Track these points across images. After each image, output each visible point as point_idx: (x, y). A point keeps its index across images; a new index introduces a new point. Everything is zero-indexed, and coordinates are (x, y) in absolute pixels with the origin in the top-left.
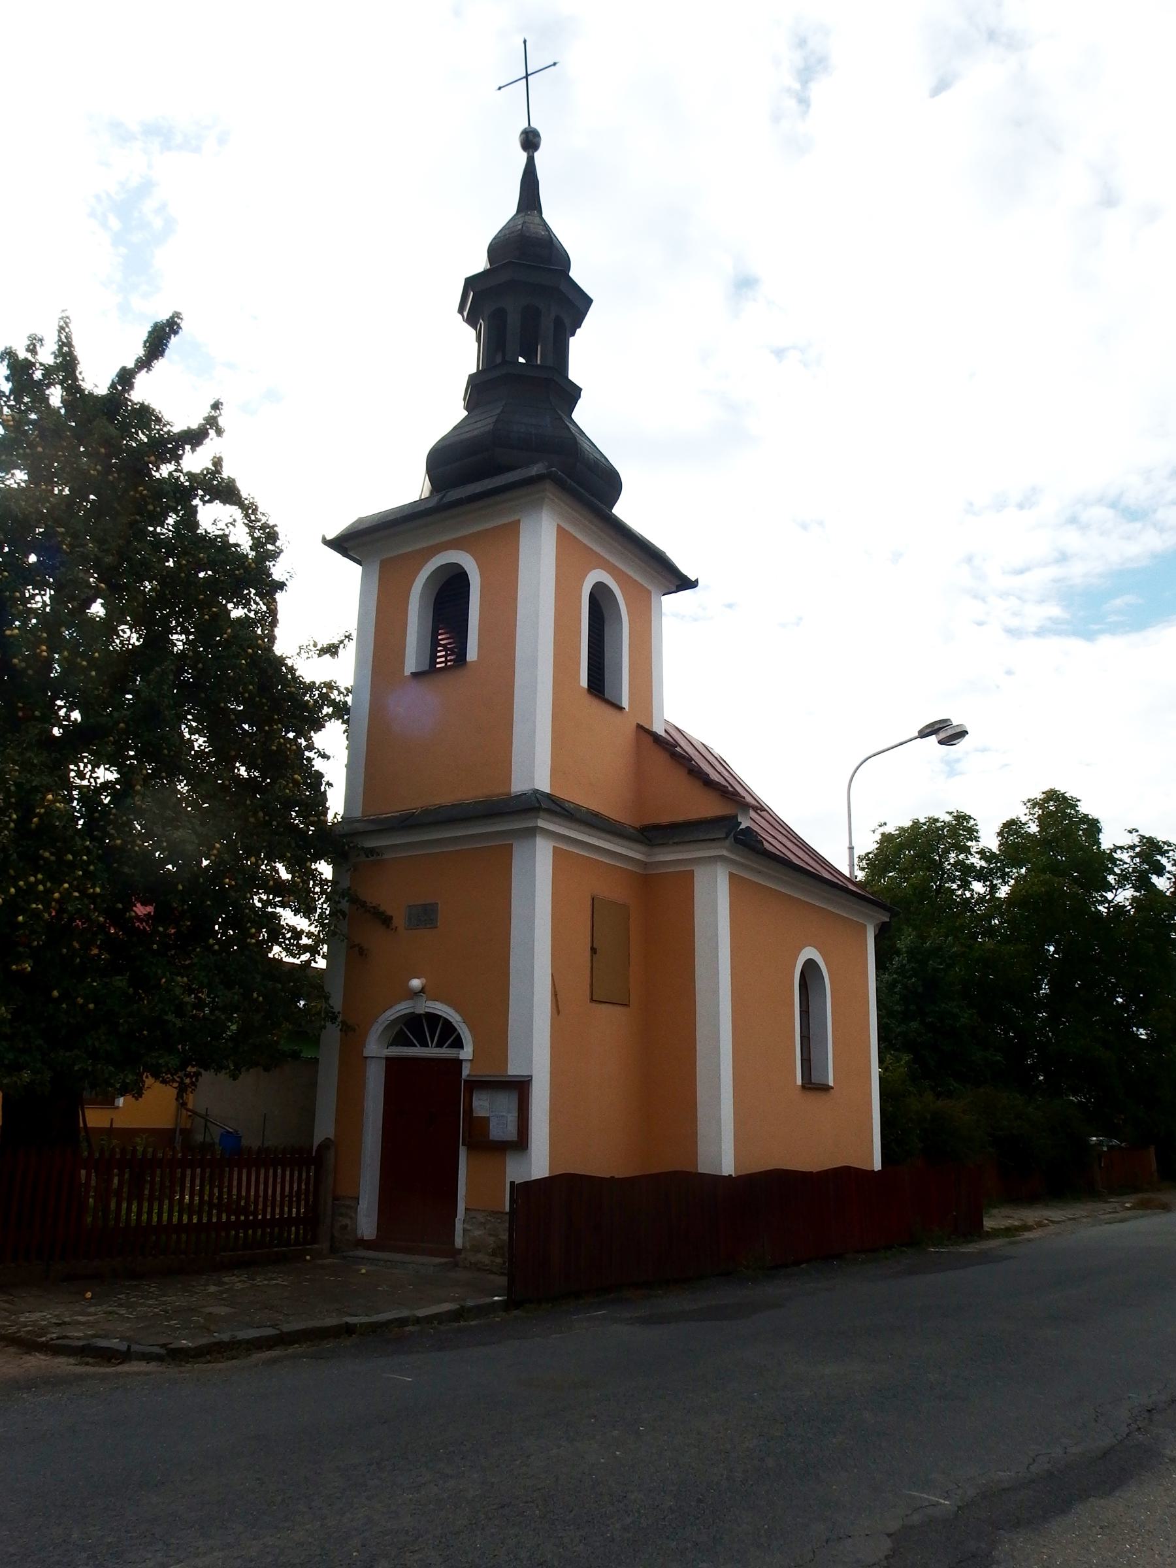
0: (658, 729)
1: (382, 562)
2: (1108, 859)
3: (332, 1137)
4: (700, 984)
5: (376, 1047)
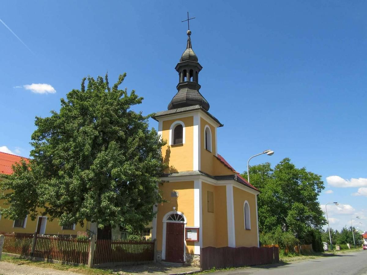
0: (217, 156)
1: (164, 122)
2: (126, 113)
3: (156, 238)
4: (201, 205)
5: (165, 220)
